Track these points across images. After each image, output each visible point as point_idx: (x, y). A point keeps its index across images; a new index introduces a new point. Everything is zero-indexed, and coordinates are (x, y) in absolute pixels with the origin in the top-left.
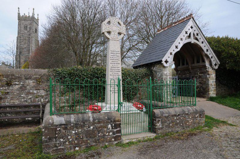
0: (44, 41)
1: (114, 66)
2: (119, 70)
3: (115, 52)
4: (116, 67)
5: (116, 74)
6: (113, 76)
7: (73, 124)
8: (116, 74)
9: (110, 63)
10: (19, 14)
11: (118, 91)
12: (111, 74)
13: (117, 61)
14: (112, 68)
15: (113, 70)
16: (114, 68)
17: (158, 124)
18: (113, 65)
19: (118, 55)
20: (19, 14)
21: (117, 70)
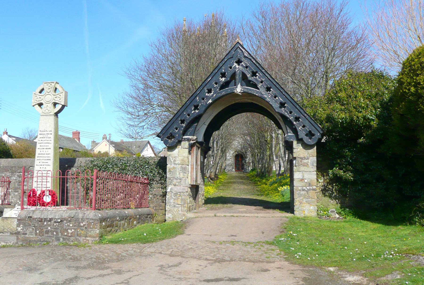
0: (194, 146)
1: (43, 153)
2: (49, 158)
3: (45, 133)
4: (46, 153)
5: (43, 164)
6: (41, 166)
7: (406, 220)
8: (43, 164)
9: (37, 148)
10: (58, 104)
11: (24, 185)
12: (38, 164)
13: (47, 144)
14: (40, 156)
15: (41, 158)
16: (42, 156)
17: (19, 228)
18: (42, 150)
19: (50, 137)
20: (58, 104)
21: (47, 158)
